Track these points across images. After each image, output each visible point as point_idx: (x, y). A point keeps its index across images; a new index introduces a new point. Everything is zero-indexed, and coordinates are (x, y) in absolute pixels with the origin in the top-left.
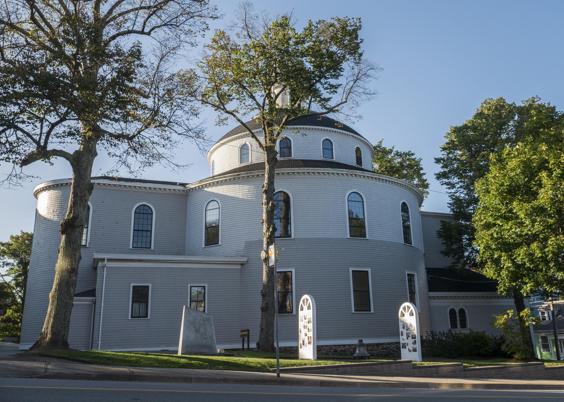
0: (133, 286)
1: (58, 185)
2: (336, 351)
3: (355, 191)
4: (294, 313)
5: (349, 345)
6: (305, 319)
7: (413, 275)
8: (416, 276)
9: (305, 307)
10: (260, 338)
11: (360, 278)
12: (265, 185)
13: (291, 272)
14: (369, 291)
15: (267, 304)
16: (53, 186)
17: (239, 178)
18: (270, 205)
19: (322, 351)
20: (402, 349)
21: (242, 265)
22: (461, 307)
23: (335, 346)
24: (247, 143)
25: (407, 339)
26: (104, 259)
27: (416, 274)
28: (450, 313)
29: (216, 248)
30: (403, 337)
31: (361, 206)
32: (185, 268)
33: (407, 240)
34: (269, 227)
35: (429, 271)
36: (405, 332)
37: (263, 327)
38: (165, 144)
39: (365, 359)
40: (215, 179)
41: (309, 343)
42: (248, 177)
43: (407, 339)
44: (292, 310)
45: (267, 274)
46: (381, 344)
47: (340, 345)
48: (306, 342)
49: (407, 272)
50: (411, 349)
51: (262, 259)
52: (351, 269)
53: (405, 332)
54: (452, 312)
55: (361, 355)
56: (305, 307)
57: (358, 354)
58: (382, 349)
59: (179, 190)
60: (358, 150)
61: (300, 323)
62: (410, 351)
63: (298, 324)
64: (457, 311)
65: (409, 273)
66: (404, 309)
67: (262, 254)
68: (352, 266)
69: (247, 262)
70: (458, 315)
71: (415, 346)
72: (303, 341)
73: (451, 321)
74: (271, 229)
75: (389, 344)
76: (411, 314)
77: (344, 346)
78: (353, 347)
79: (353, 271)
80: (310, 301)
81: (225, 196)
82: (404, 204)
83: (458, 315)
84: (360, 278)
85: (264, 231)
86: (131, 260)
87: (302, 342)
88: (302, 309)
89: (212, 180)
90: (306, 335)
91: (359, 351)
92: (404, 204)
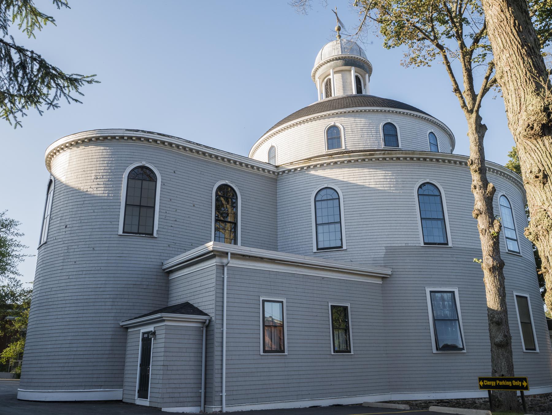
0: (331, 306)
1: (105, 138)
14: (531, 323)
16: (97, 139)
24: (338, 124)
26: (227, 253)
29: (337, 253)
32: (323, 278)
40: (334, 158)
42: (384, 159)
59: (269, 171)
78: (530, 399)
86: (261, 259)
89: (329, 159)
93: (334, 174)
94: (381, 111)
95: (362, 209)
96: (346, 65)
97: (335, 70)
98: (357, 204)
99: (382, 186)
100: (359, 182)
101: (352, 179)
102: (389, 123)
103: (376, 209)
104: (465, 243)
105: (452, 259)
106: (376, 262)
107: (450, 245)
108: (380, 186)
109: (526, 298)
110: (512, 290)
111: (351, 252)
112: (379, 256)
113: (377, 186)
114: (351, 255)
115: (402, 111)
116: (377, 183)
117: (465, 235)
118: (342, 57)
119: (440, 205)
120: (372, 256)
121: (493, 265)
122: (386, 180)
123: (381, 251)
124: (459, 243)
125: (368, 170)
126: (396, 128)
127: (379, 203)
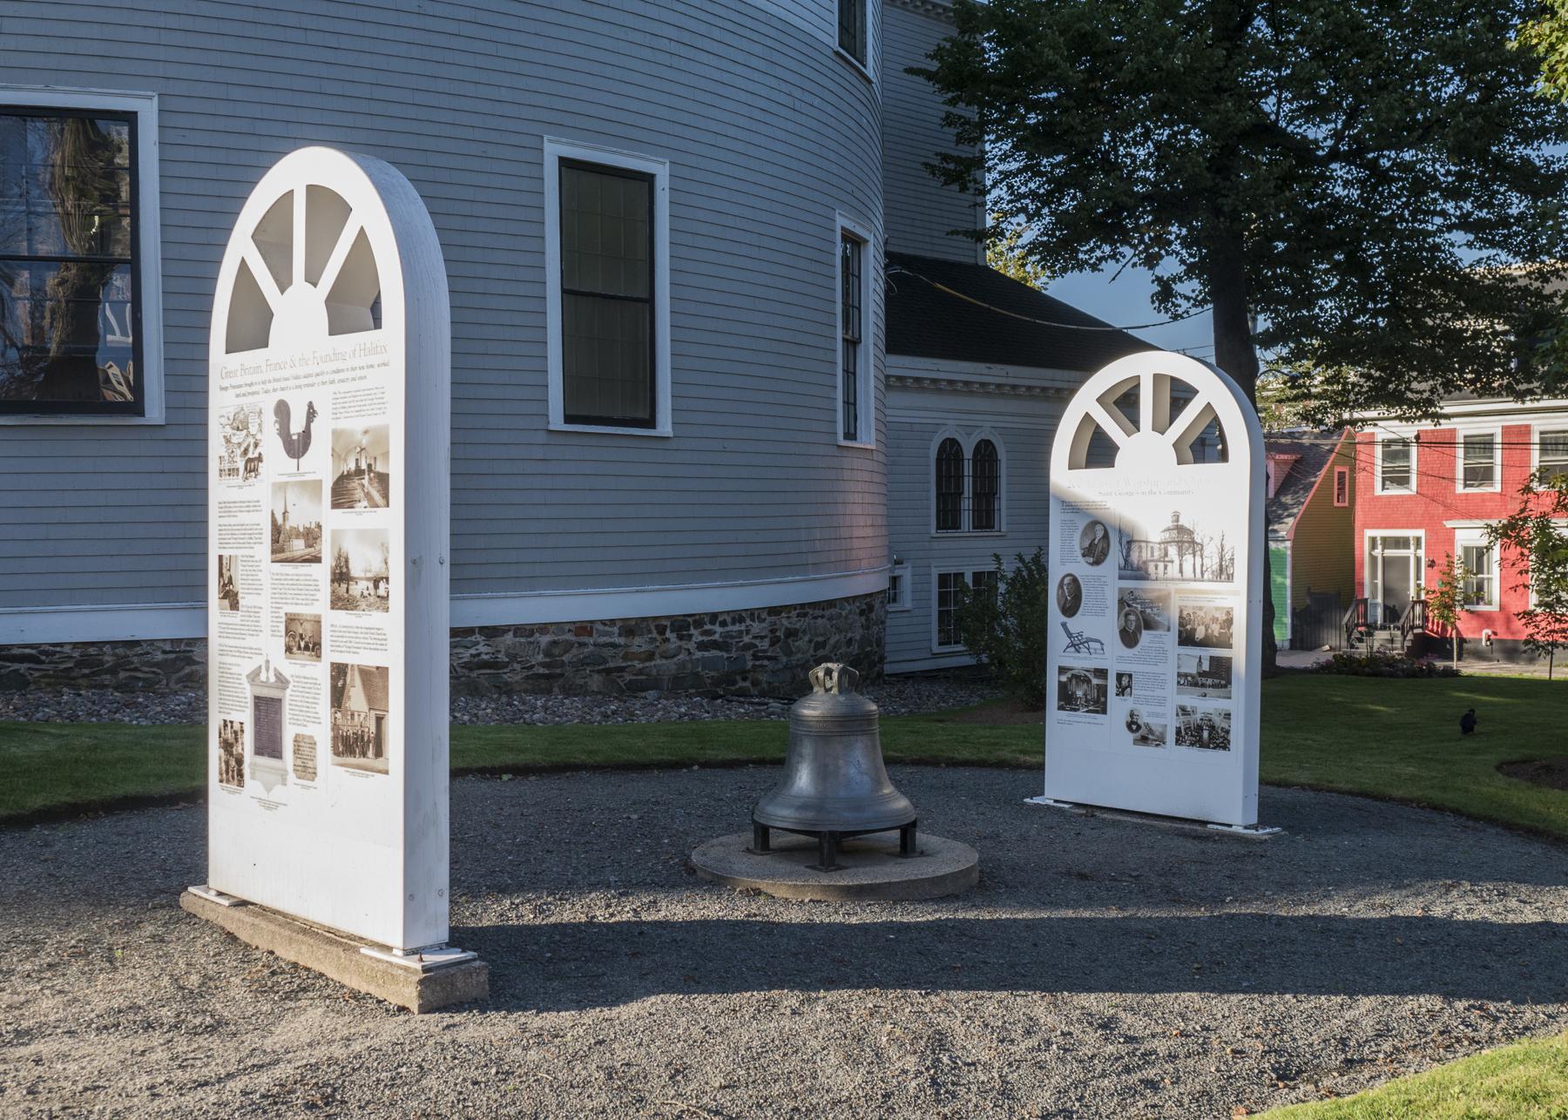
4: (155, 411)
5: (519, 630)
6: (297, 446)
9: (299, 309)
13: (130, 118)
14: (650, 301)
22: (947, 435)
28: (939, 461)
30: (1076, 624)
36: (1102, 585)
38: (602, 1075)
41: (355, 745)
43: (1129, 638)
44: (138, 388)
46: (698, 620)
48: (309, 718)
49: (841, 221)
52: (554, 150)
53: (1102, 585)
54: (949, 453)
55: (841, 820)
56: (299, 309)
57: (816, 804)
58: (702, 646)
61: (220, 490)
62: (1143, 735)
63: (204, 489)
64: (968, 453)
65: (849, 225)
66: (1125, 402)
68: (560, 129)
70: (968, 469)
71: (1206, 705)
72: (267, 710)
73: (939, 495)
75: (738, 617)
76: (1206, 445)
78: (545, 640)
83: (968, 469)
87: (244, 716)
88: (253, 328)
91: (823, 773)
109: (649, 179)
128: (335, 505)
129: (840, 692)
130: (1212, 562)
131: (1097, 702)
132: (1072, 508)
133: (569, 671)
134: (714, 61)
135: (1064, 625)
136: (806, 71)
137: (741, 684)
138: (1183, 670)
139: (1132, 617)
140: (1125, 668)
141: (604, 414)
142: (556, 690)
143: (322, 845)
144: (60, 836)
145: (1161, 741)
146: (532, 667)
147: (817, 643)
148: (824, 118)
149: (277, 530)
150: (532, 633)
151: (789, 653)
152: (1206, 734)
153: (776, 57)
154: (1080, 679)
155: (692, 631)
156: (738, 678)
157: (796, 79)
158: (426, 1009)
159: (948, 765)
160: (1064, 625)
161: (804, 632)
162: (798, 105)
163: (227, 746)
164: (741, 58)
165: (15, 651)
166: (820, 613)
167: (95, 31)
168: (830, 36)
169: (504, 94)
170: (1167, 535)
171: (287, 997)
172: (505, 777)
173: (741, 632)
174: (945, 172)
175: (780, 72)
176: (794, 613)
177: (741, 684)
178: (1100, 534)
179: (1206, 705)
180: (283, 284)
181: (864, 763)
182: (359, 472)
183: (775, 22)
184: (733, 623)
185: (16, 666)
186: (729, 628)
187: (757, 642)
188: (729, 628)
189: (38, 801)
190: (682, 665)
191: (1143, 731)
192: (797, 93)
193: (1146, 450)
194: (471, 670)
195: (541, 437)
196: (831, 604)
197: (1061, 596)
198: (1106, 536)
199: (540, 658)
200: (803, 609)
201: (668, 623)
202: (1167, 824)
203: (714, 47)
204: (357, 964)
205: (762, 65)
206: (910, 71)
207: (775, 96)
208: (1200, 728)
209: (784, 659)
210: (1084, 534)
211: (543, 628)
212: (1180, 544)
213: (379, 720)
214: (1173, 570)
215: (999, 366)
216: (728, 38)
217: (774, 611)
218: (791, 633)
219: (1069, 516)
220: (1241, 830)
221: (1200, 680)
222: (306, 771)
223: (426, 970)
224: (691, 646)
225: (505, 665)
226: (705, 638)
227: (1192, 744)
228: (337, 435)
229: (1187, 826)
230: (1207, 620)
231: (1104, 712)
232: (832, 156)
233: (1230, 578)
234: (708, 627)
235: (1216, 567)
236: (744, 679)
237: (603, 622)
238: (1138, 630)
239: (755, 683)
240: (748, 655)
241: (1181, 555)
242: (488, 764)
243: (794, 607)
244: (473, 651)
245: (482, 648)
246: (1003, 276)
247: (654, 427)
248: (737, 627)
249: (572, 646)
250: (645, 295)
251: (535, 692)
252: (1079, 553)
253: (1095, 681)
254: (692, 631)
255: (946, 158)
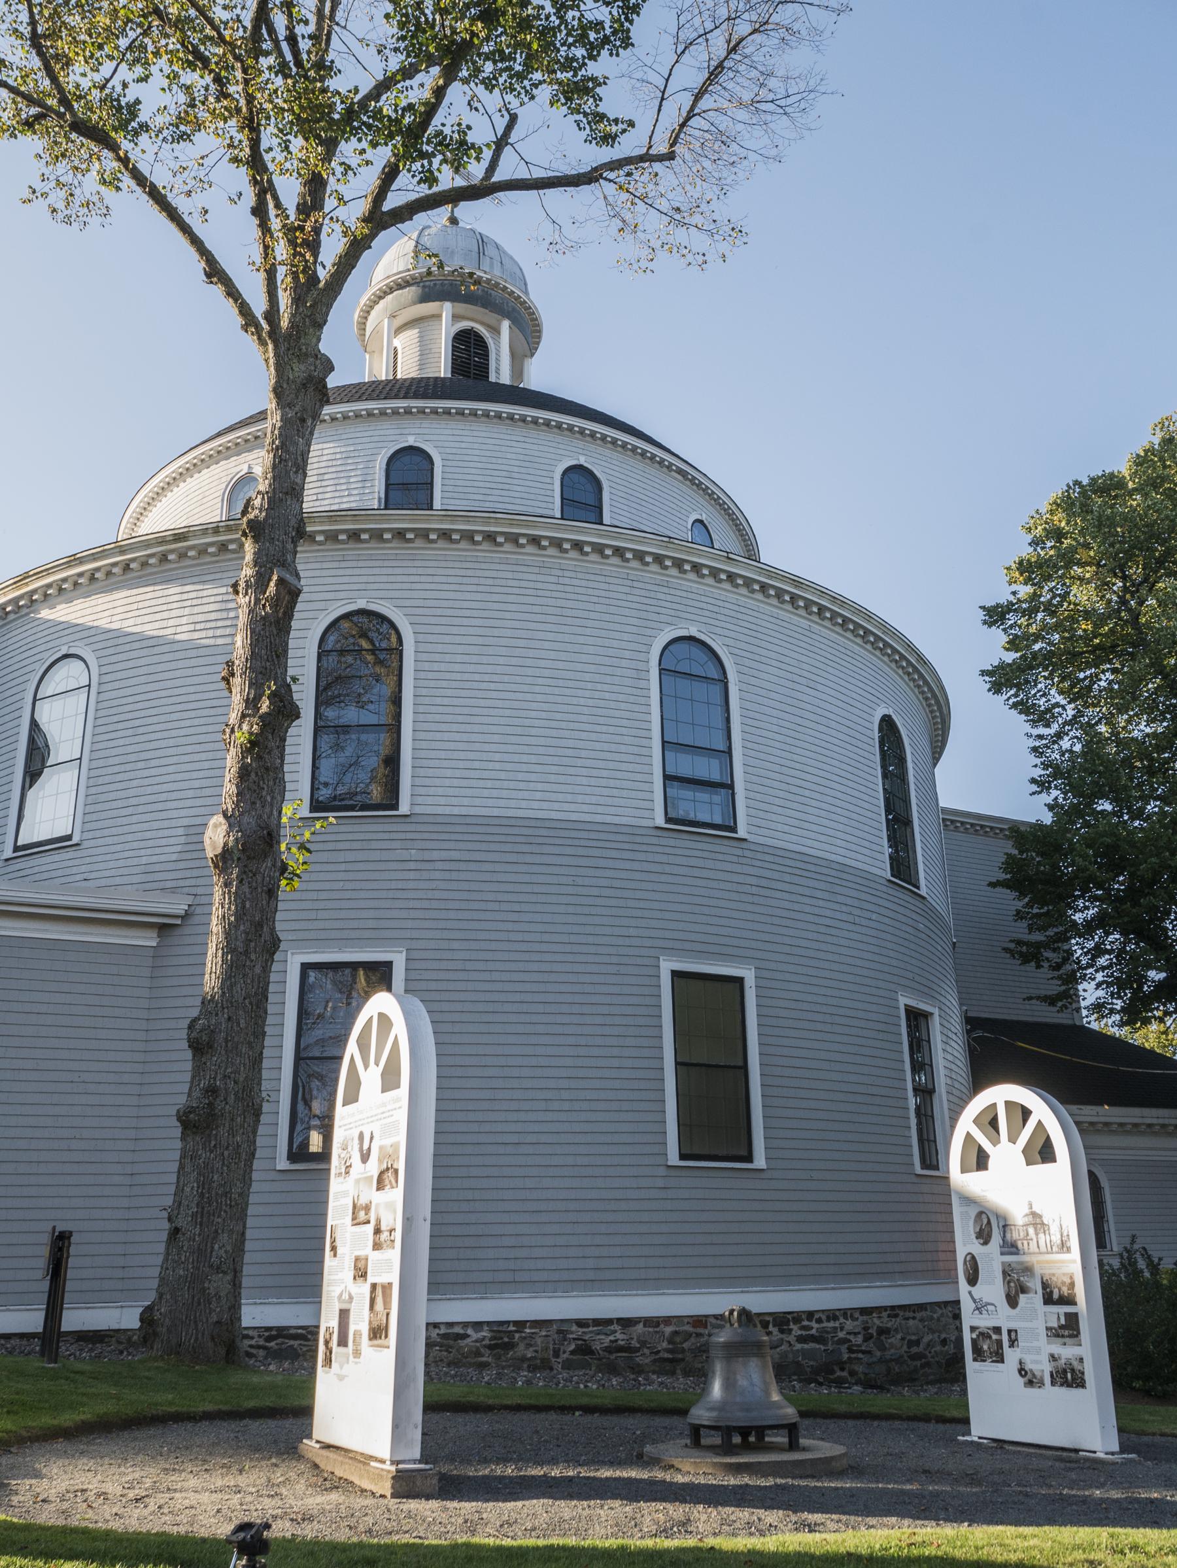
2: (585, 1349)
3: (693, 632)
5: (649, 1322)
6: (365, 1157)
7: (926, 1016)
8: (936, 1018)
9: (371, 1077)
10: (162, 1280)
11: (708, 1007)
12: (257, 502)
14: (744, 1068)
15: (212, 1091)
17: (183, 555)
18: (272, 588)
19: (521, 1350)
20: (971, 1366)
21: (164, 929)
23: (581, 1323)
25: (1012, 1301)
27: (936, 1011)
30: (979, 1291)
31: (718, 699)
33: (903, 868)
34: (258, 698)
35: (972, 1023)
36: (991, 1258)
37: (181, 1222)
39: (762, 1446)
43: (1012, 1301)
45: (227, 935)
46: (797, 1317)
47: (609, 1322)
49: (903, 1001)
50: (1044, 1368)
51: (210, 854)
52: (667, 966)
53: (991, 1258)
55: (740, 1418)
56: (371, 1077)
57: (721, 1407)
60: (693, 669)
62: (1032, 1380)
66: (990, 1122)
67: (209, 833)
68: (671, 951)
69: (186, 916)
71: (1067, 1352)
72: (344, 1314)
74: (265, 705)
75: (832, 1315)
76: (1043, 1152)
77: (626, 1323)
78: (668, 1330)
79: (675, 974)
80: (400, 1029)
81: (119, 634)
82: (887, 724)
84: (708, 1007)
85: (233, 718)
87: (334, 1323)
90: (361, 1273)
91: (728, 1385)
92: (887, 724)
93: (89, 611)
94: (408, 411)
95: (143, 714)
96: (425, 298)
97: (398, 322)
98: (130, 700)
99: (210, 633)
100: (150, 629)
101: (79, 614)
102: (411, 448)
103: (179, 707)
104: (466, 801)
105: (405, 855)
106: (150, 877)
107: (742, 832)
108: (203, 634)
109: (740, 981)
110: (652, 952)
111: (90, 852)
112: (163, 858)
113: (196, 635)
114: (88, 860)
115: (519, 410)
116: (198, 627)
117: (472, 774)
118: (413, 277)
119: (718, 711)
120: (144, 860)
121: (226, 844)
122: (224, 615)
123: (172, 841)
124: (442, 801)
125: (179, 589)
126: (432, 463)
127: (192, 689)
128: (378, 1189)
129: (740, 1326)
130: (1056, 1239)
131: (997, 1353)
132: (968, 1200)
133: (689, 1357)
134: (786, 896)
135: (970, 1293)
136: (863, 896)
137: (839, 1373)
138: (1050, 1325)
139: (1012, 1284)
140: (1013, 1325)
141: (713, 1152)
142: (678, 1371)
143: (360, 1403)
144: (255, 1425)
145: (1041, 1384)
146: (659, 1352)
147: (909, 1341)
148: (883, 927)
149: (355, 1206)
150: (658, 1324)
151: (883, 1348)
152: (1069, 1376)
153: (838, 889)
154: (984, 1335)
155: (792, 1326)
156: (836, 1368)
157: (856, 903)
158: (394, 1496)
159: (937, 1422)
160: (970, 1293)
161: (896, 1330)
162: (857, 920)
163: (327, 1343)
164: (807, 892)
165: (292, 1331)
166: (911, 1314)
167: (371, 914)
168: (884, 870)
169: (632, 932)
170: (1026, 1219)
171: (326, 1490)
172: (577, 1413)
173: (835, 1328)
174: (1021, 954)
175: (840, 899)
176: (885, 1314)
177: (839, 1373)
178: (985, 1221)
179: (1067, 1352)
180: (366, 1066)
181: (756, 1377)
182: (388, 1169)
183: (834, 866)
184: (828, 1320)
185: (292, 1342)
186: (825, 1324)
187: (851, 1337)
188: (825, 1324)
189: (251, 1404)
190: (784, 1355)
191: (1029, 1376)
192: (857, 912)
193: (1006, 1154)
194: (610, 1352)
195: (662, 1171)
196: (922, 1307)
197: (966, 1271)
198: (989, 1222)
199: (665, 1345)
200: (894, 1311)
201: (771, 1319)
202: (1032, 1450)
203: (787, 887)
204: (368, 1472)
205: (826, 896)
206: (992, 885)
207: (838, 916)
208: (1065, 1371)
209: (878, 1354)
210: (975, 1221)
211: (668, 1320)
212: (1035, 1225)
213: (388, 1314)
214: (1033, 1245)
215: (1089, 1107)
216: (796, 880)
217: (865, 1311)
218: (882, 1331)
219: (965, 1209)
220: (1101, 1455)
221: (1061, 1332)
222: (357, 1353)
223: (398, 1471)
224: (792, 1339)
225: (637, 1350)
226: (804, 1333)
227: (1062, 1385)
228: (381, 1148)
229: (1065, 1454)
230: (1059, 1284)
231: (1003, 1362)
232: (892, 954)
233: (1069, 1250)
234: (806, 1323)
235: (1059, 1242)
236: (842, 1369)
237: (716, 1317)
238: (1017, 1294)
239: (852, 1373)
240: (844, 1348)
241: (1037, 1234)
242: (567, 1404)
243: (885, 1308)
244: (612, 1338)
245: (619, 1336)
246: (1105, 1035)
247: (751, 1161)
248: (831, 1324)
249: (691, 1335)
250: (741, 1063)
251: (659, 1373)
252: (973, 1236)
253: (994, 1337)
254: (792, 1326)
255: (1019, 942)
